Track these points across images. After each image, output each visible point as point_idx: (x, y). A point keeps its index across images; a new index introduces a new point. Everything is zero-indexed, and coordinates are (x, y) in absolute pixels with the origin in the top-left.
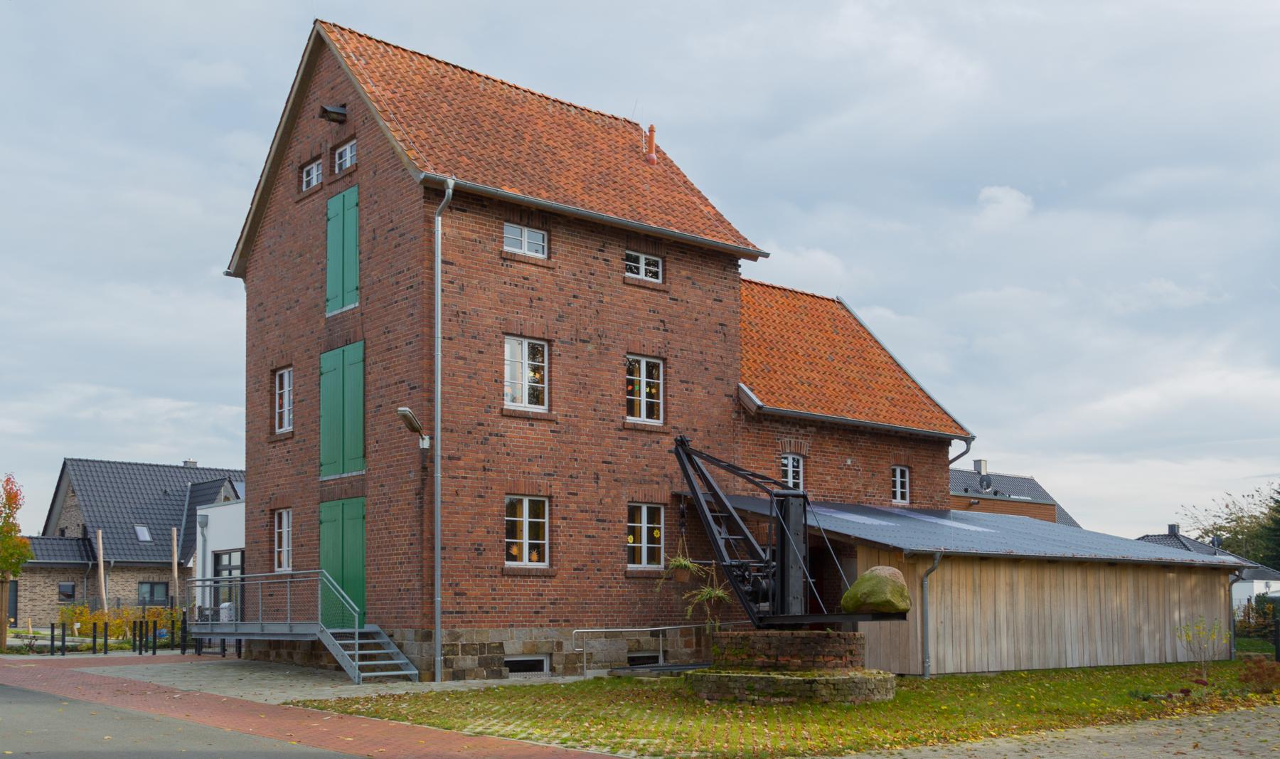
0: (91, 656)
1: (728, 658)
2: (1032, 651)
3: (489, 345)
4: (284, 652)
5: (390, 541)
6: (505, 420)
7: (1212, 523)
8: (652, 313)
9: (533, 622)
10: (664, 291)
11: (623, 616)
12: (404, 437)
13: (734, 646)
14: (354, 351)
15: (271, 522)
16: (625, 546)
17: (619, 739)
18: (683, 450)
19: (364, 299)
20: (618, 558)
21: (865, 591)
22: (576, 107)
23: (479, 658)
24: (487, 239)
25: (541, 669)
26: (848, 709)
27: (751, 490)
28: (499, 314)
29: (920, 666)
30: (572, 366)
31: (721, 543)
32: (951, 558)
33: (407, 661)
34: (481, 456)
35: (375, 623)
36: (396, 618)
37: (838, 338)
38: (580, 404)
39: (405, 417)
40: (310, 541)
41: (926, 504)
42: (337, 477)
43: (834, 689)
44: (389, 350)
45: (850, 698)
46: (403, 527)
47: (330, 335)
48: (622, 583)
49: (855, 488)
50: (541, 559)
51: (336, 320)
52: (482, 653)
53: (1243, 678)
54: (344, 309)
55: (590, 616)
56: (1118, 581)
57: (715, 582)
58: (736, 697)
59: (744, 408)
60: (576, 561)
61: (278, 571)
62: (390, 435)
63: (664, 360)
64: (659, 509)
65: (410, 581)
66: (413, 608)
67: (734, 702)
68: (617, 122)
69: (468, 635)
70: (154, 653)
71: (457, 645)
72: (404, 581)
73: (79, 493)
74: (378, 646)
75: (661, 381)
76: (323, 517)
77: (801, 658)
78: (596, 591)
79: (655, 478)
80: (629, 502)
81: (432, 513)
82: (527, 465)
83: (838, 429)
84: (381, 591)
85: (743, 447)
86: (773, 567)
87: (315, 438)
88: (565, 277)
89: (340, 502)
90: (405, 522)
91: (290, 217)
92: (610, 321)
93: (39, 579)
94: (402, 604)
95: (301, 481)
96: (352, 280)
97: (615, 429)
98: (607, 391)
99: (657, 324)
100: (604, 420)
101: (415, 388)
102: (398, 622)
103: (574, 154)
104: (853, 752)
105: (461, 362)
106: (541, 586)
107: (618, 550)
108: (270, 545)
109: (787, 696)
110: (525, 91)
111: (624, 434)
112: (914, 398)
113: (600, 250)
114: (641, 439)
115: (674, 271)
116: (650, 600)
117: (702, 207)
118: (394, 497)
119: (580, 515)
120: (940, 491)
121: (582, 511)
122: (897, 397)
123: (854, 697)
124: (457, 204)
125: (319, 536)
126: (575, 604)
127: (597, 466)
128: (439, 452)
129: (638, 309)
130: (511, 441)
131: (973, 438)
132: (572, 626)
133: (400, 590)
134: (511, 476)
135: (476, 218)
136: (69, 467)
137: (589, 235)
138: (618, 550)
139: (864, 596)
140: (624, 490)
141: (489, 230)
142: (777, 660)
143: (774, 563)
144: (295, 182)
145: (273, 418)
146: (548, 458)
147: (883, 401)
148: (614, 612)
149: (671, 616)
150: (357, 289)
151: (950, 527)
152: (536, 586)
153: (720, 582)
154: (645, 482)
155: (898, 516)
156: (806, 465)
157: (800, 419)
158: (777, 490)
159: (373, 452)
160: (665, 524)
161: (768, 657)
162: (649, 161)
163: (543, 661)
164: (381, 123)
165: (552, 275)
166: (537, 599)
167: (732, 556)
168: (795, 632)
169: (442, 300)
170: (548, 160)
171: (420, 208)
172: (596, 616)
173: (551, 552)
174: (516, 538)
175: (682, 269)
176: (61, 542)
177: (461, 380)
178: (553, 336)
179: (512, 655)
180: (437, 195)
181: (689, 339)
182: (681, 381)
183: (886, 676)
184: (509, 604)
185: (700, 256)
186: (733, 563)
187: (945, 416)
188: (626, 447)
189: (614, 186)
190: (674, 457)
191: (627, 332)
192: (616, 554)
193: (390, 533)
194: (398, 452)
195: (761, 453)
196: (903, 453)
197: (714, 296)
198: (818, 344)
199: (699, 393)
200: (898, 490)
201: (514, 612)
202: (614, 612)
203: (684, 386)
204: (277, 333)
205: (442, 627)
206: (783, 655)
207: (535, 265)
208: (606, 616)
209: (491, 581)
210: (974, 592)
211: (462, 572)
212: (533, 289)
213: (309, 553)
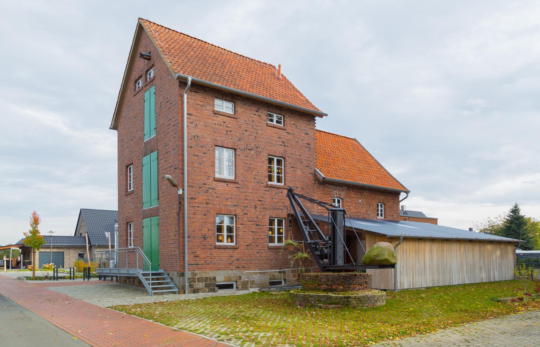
0: (69, 281)
1: (309, 285)
2: (439, 278)
3: (209, 150)
4: (131, 280)
5: (168, 234)
6: (216, 182)
7: (483, 228)
8: (279, 138)
9: (229, 268)
10: (284, 129)
11: (267, 265)
12: (172, 190)
13: (312, 280)
14: (154, 155)
15: (126, 228)
16: (268, 236)
17: (250, 333)
18: (291, 193)
19: (158, 133)
20: (265, 241)
21: (375, 254)
22: (249, 59)
23: (205, 284)
24: (207, 105)
25: (233, 288)
26: (366, 310)
27: (320, 213)
28: (213, 137)
29: (393, 286)
30: (245, 160)
31: (307, 233)
32: (407, 239)
33: (174, 285)
34: (206, 198)
35: (163, 269)
36: (170, 267)
37: (355, 153)
38: (248, 176)
39: (168, 179)
40: (140, 235)
41: (390, 218)
42: (149, 208)
43: (359, 301)
44: (167, 153)
45: (366, 305)
46: (172, 228)
47: (146, 149)
48: (267, 251)
49: (362, 212)
50: (232, 241)
51: (148, 143)
52: (206, 281)
53: (536, 290)
54: (151, 138)
55: (253, 265)
56: (473, 248)
57: (304, 251)
58: (312, 305)
59: (317, 179)
60: (247, 242)
61: (130, 247)
62: (167, 189)
63: (284, 158)
64: (282, 220)
65: (175, 251)
66: (176, 263)
67: (311, 307)
68: (266, 65)
69: (200, 274)
70: (88, 280)
71: (195, 278)
72: (173, 251)
73: (85, 221)
74: (164, 279)
75: (283, 167)
76: (144, 225)
77: (343, 286)
78: (256, 255)
79: (280, 208)
80: (269, 217)
81: (184, 222)
82: (225, 201)
83: (356, 188)
84: (165, 255)
85: (317, 195)
86: (330, 243)
87: (141, 193)
88: (241, 122)
89: (150, 218)
90: (173, 226)
91: (132, 103)
92: (261, 141)
93: (71, 251)
94: (172, 261)
95: (136, 211)
96: (153, 126)
97: (263, 187)
98: (260, 171)
99: (281, 143)
100: (259, 183)
101: (176, 168)
102: (171, 269)
103: (247, 74)
104: (374, 343)
105: (196, 157)
106: (232, 253)
107: (265, 237)
108: (126, 237)
109: (336, 304)
110: (228, 51)
111: (267, 189)
112: (386, 176)
113: (256, 111)
114: (274, 191)
115: (288, 121)
116: (278, 258)
117: (300, 97)
118: (169, 216)
119: (248, 223)
120: (396, 213)
121: (249, 221)
122: (379, 175)
123: (368, 304)
124: (193, 90)
125: (143, 233)
126: (247, 260)
127: (256, 202)
128: (186, 196)
129: (273, 137)
130: (218, 191)
131: (409, 192)
132: (245, 269)
133: (171, 255)
134: (219, 207)
135: (202, 96)
136: (82, 212)
137: (252, 105)
138: (265, 237)
139: (374, 257)
140: (267, 212)
141: (208, 101)
142: (332, 287)
143: (330, 242)
144: (133, 88)
145: (127, 185)
146: (235, 199)
147: (374, 177)
148: (263, 263)
149: (287, 265)
150: (155, 129)
151: (400, 226)
152: (230, 253)
153: (306, 250)
154: (277, 209)
155: (380, 222)
156: (343, 202)
157: (340, 184)
158: (331, 208)
159: (161, 197)
160: (285, 227)
161: (327, 285)
162: (279, 79)
163: (233, 284)
164: (162, 56)
165: (236, 121)
166: (230, 258)
167: (311, 239)
168: (340, 273)
169: (187, 130)
170: (236, 75)
171: (178, 91)
172: (256, 265)
173: (236, 238)
174: (231, 233)
175: (292, 120)
176: (81, 238)
177: (196, 165)
178: (236, 147)
179: (220, 282)
180: (185, 85)
181: (294, 150)
182: (291, 167)
183: (382, 294)
184: (218, 260)
185: (299, 115)
186: (312, 242)
187: (398, 183)
188: (268, 194)
189: (263, 86)
190: (287, 199)
191: (268, 146)
192: (264, 239)
193: (168, 231)
194: (170, 196)
195: (324, 197)
196: (381, 197)
197: (305, 132)
198: (347, 155)
199: (299, 172)
200: (380, 213)
201: (220, 264)
202: (263, 263)
203: (292, 169)
204: (128, 151)
205: (188, 271)
206: (334, 285)
207: (229, 117)
208: (260, 265)
209: (210, 251)
210: (416, 253)
211: (197, 247)
212: (227, 127)
213: (139, 240)
